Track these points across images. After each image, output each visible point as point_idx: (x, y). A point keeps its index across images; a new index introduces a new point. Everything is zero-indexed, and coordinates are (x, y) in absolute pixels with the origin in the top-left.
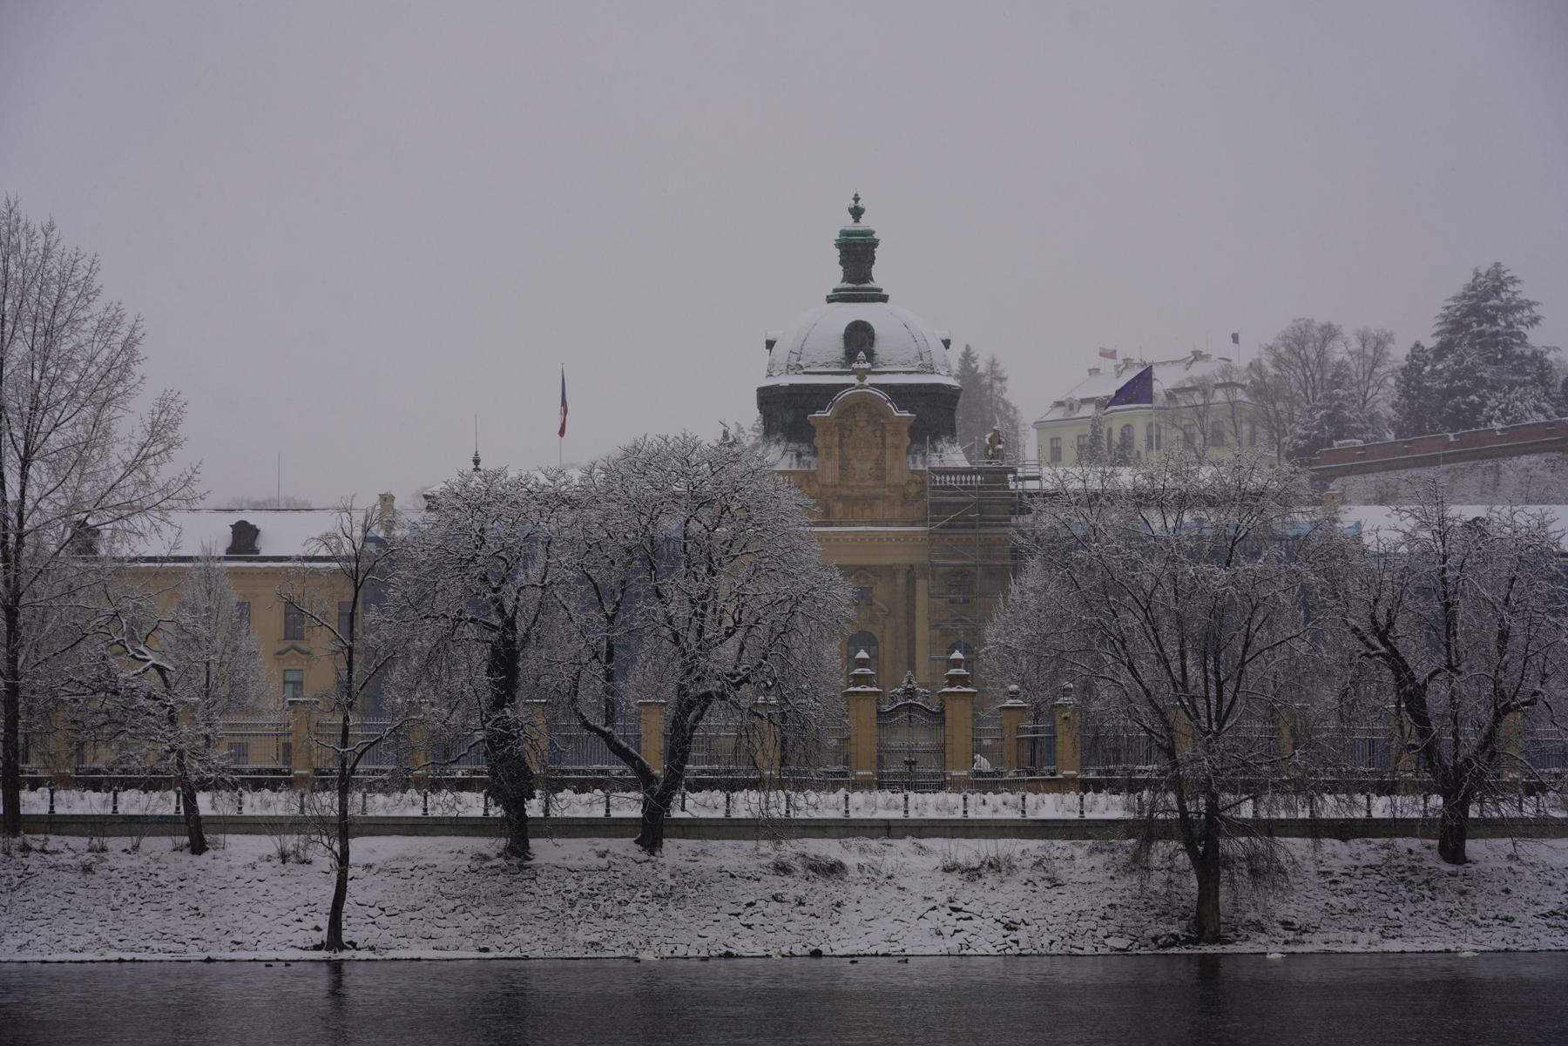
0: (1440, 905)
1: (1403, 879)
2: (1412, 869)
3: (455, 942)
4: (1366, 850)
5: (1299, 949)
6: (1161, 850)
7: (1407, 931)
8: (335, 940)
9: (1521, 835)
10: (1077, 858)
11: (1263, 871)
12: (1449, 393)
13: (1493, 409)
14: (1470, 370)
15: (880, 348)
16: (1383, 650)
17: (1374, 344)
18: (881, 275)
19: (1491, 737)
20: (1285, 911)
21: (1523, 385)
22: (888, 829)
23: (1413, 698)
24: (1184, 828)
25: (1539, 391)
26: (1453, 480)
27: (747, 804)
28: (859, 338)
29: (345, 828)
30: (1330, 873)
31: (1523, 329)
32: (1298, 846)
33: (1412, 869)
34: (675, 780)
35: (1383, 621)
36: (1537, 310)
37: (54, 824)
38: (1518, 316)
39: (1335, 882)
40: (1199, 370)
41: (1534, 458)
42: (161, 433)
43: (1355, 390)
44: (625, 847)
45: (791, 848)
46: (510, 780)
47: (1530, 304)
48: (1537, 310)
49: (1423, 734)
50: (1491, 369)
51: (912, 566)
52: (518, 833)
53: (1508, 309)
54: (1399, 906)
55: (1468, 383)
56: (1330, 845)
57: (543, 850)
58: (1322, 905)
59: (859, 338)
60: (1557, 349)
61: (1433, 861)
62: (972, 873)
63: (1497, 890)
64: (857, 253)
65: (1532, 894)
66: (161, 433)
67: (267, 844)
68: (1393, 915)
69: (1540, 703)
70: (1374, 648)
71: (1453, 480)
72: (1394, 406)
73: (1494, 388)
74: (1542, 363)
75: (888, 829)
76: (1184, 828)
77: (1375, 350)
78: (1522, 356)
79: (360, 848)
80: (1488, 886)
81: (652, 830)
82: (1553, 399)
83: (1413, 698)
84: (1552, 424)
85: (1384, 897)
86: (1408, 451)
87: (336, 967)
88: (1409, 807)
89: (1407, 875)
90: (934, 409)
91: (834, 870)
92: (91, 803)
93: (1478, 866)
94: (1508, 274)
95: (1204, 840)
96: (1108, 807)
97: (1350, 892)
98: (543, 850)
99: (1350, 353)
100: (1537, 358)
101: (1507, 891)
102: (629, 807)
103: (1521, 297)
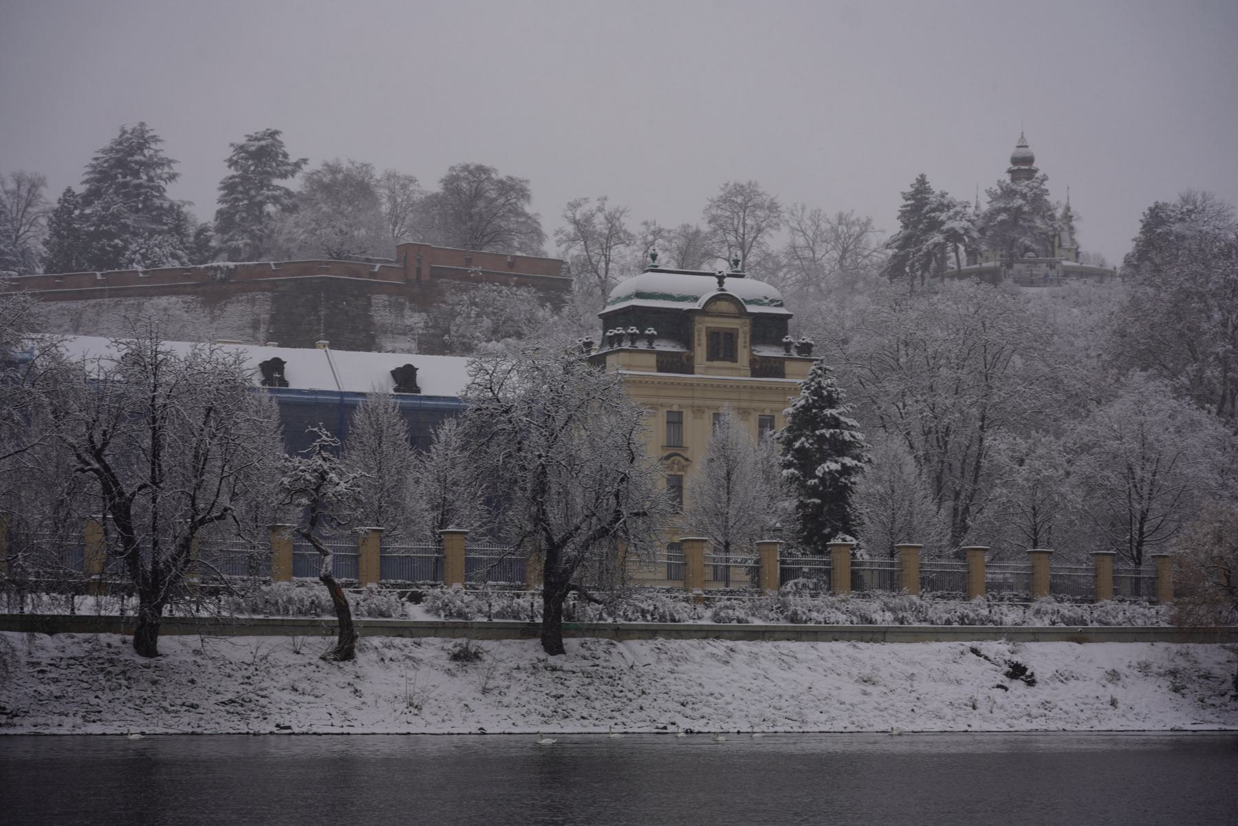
0: (135, 693)
1: (102, 670)
2: (111, 661)
4: (73, 644)
5: (11, 731)
7: (105, 716)
9: (209, 633)
12: (97, 236)
13: (135, 253)
14: (116, 217)
16: (97, 466)
17: (28, 186)
19: (186, 546)
21: (160, 233)
23: (121, 513)
25: (175, 240)
26: (98, 314)
30: (39, 664)
31: (162, 183)
33: (111, 661)
35: (97, 437)
36: (176, 168)
38: (159, 171)
39: (43, 672)
41: (174, 299)
43: (9, 226)
47: (170, 162)
48: (176, 168)
49: (129, 541)
50: (134, 216)
51: (668, 422)
53: (150, 165)
54: (99, 693)
55: (114, 229)
56: (44, 639)
58: (30, 692)
60: (190, 203)
61: (129, 654)
63: (184, 681)
65: (214, 685)
68: (94, 701)
69: (230, 519)
70: (88, 464)
71: (98, 314)
72: (46, 243)
73: (135, 234)
74: (178, 214)
77: (29, 191)
78: (161, 208)
80: (177, 677)
82: (186, 248)
83: (121, 513)
84: (188, 270)
85: (85, 685)
86: (59, 285)
93: (168, 659)
94: (151, 133)
97: (56, 681)
99: (6, 192)
100: (1127, 262)
101: (193, 682)
103: (161, 154)
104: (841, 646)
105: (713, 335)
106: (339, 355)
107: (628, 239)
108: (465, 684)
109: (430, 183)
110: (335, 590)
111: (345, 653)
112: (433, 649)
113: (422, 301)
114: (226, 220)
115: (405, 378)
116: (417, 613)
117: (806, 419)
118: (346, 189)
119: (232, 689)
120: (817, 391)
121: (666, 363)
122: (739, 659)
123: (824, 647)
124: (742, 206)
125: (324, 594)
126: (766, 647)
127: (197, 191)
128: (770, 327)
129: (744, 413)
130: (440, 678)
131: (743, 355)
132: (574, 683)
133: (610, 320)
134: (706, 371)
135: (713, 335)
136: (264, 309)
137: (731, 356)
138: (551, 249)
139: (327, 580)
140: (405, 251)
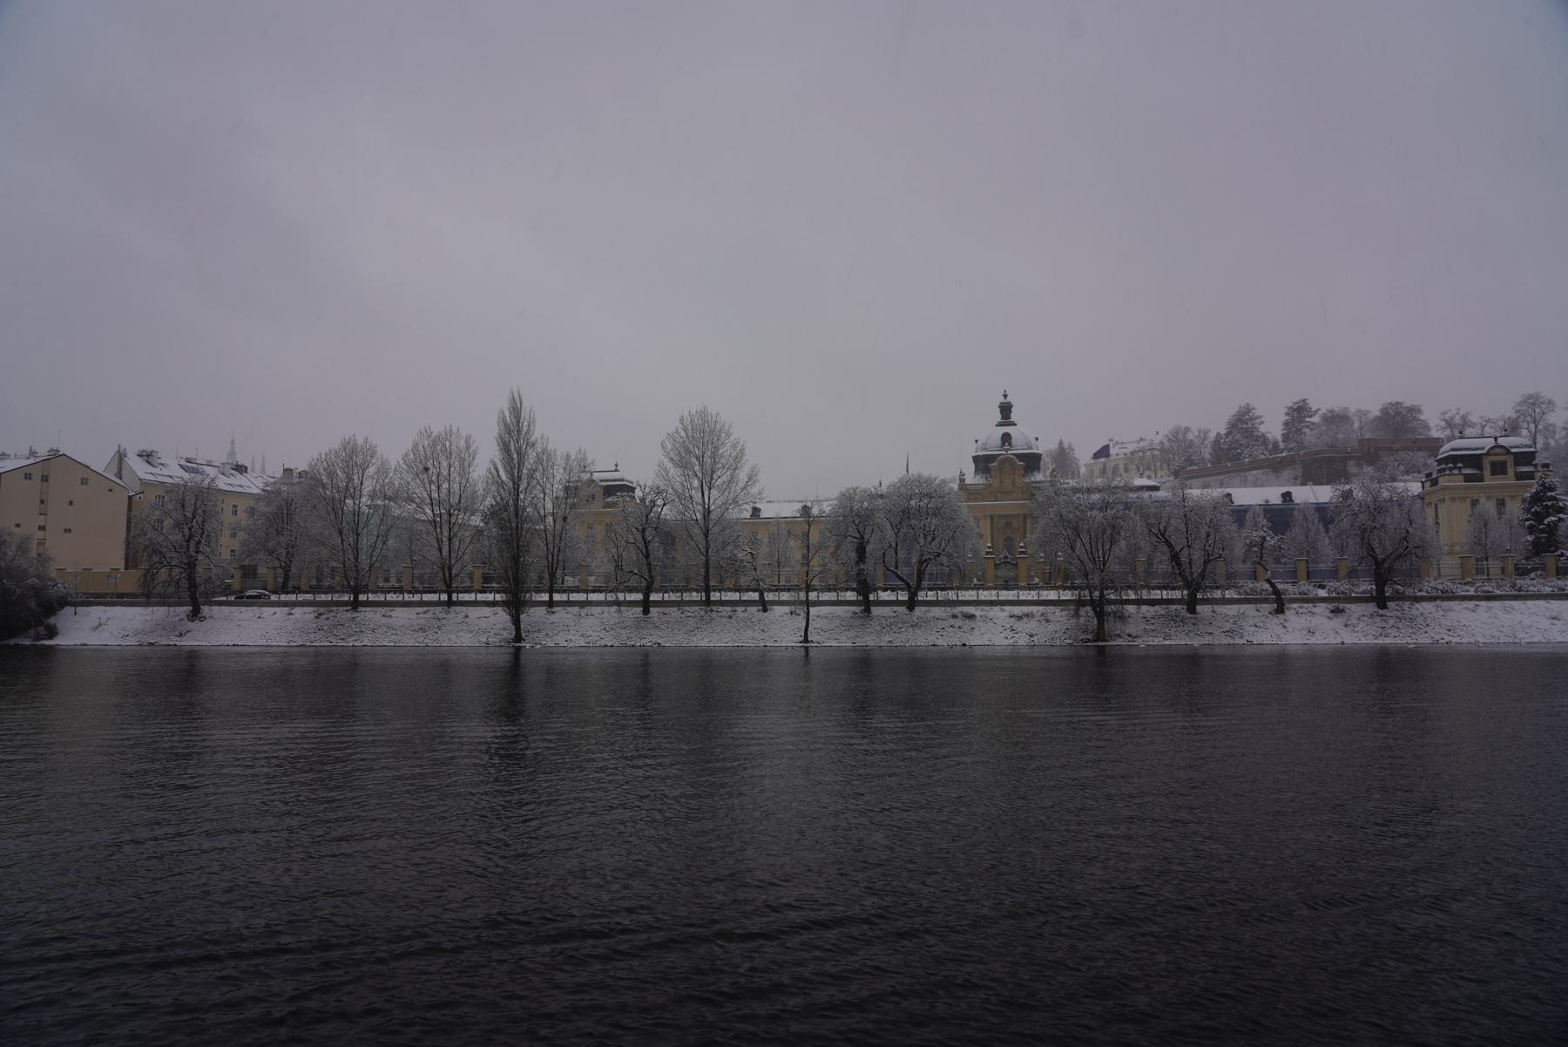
3: (845, 641)
6: (1082, 611)
8: (806, 640)
10: (1057, 613)
11: (1122, 618)
15: (1014, 441)
18: (1014, 417)
20: (1128, 631)
22: (992, 603)
24: (1092, 602)
27: (942, 595)
28: (1006, 438)
29: (808, 604)
32: (1131, 609)
34: (919, 588)
37: (722, 603)
40: (1142, 444)
42: (751, 478)
44: (902, 609)
45: (958, 610)
46: (864, 588)
52: (867, 605)
53: (1252, 419)
56: (1144, 608)
57: (875, 611)
59: (1006, 438)
61: (1185, 613)
62: (1019, 618)
64: (1006, 409)
66: (751, 478)
67: (787, 609)
75: (992, 603)
76: (1092, 602)
79: (813, 611)
81: (911, 604)
83: (1175, 557)
87: (518, 649)
88: (1176, 594)
89: (1174, 619)
90: (1032, 461)
91: (972, 617)
92: (735, 596)
95: (1099, 606)
96: (1067, 595)
98: (875, 611)
102: (903, 596)
104: (1541, 603)
105: (1493, 464)
106: (1317, 488)
107: (1472, 425)
108: (1337, 623)
109: (1375, 412)
110: (1272, 585)
111: (1280, 610)
112: (1322, 608)
113: (1371, 462)
114: (1286, 437)
115: (1287, 496)
116: (1323, 593)
117: (1536, 498)
118: (1336, 419)
119: (1228, 626)
120: (1543, 485)
121: (1468, 478)
122: (1480, 610)
123: (1530, 603)
124: (1534, 406)
125: (1267, 586)
126: (1497, 604)
127: (1272, 426)
128: (1526, 458)
129: (1489, 498)
130: (1325, 621)
131: (1511, 471)
132: (1391, 622)
133: (1440, 462)
134: (1490, 480)
135: (1493, 464)
136: (1299, 472)
137: (1504, 472)
138: (1435, 434)
139: (1268, 581)
140: (1362, 441)
